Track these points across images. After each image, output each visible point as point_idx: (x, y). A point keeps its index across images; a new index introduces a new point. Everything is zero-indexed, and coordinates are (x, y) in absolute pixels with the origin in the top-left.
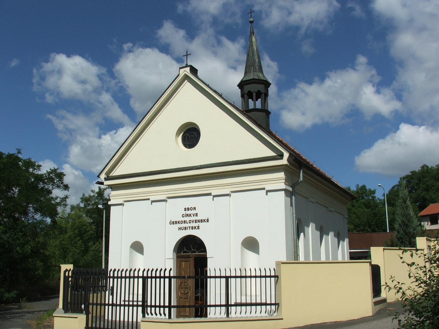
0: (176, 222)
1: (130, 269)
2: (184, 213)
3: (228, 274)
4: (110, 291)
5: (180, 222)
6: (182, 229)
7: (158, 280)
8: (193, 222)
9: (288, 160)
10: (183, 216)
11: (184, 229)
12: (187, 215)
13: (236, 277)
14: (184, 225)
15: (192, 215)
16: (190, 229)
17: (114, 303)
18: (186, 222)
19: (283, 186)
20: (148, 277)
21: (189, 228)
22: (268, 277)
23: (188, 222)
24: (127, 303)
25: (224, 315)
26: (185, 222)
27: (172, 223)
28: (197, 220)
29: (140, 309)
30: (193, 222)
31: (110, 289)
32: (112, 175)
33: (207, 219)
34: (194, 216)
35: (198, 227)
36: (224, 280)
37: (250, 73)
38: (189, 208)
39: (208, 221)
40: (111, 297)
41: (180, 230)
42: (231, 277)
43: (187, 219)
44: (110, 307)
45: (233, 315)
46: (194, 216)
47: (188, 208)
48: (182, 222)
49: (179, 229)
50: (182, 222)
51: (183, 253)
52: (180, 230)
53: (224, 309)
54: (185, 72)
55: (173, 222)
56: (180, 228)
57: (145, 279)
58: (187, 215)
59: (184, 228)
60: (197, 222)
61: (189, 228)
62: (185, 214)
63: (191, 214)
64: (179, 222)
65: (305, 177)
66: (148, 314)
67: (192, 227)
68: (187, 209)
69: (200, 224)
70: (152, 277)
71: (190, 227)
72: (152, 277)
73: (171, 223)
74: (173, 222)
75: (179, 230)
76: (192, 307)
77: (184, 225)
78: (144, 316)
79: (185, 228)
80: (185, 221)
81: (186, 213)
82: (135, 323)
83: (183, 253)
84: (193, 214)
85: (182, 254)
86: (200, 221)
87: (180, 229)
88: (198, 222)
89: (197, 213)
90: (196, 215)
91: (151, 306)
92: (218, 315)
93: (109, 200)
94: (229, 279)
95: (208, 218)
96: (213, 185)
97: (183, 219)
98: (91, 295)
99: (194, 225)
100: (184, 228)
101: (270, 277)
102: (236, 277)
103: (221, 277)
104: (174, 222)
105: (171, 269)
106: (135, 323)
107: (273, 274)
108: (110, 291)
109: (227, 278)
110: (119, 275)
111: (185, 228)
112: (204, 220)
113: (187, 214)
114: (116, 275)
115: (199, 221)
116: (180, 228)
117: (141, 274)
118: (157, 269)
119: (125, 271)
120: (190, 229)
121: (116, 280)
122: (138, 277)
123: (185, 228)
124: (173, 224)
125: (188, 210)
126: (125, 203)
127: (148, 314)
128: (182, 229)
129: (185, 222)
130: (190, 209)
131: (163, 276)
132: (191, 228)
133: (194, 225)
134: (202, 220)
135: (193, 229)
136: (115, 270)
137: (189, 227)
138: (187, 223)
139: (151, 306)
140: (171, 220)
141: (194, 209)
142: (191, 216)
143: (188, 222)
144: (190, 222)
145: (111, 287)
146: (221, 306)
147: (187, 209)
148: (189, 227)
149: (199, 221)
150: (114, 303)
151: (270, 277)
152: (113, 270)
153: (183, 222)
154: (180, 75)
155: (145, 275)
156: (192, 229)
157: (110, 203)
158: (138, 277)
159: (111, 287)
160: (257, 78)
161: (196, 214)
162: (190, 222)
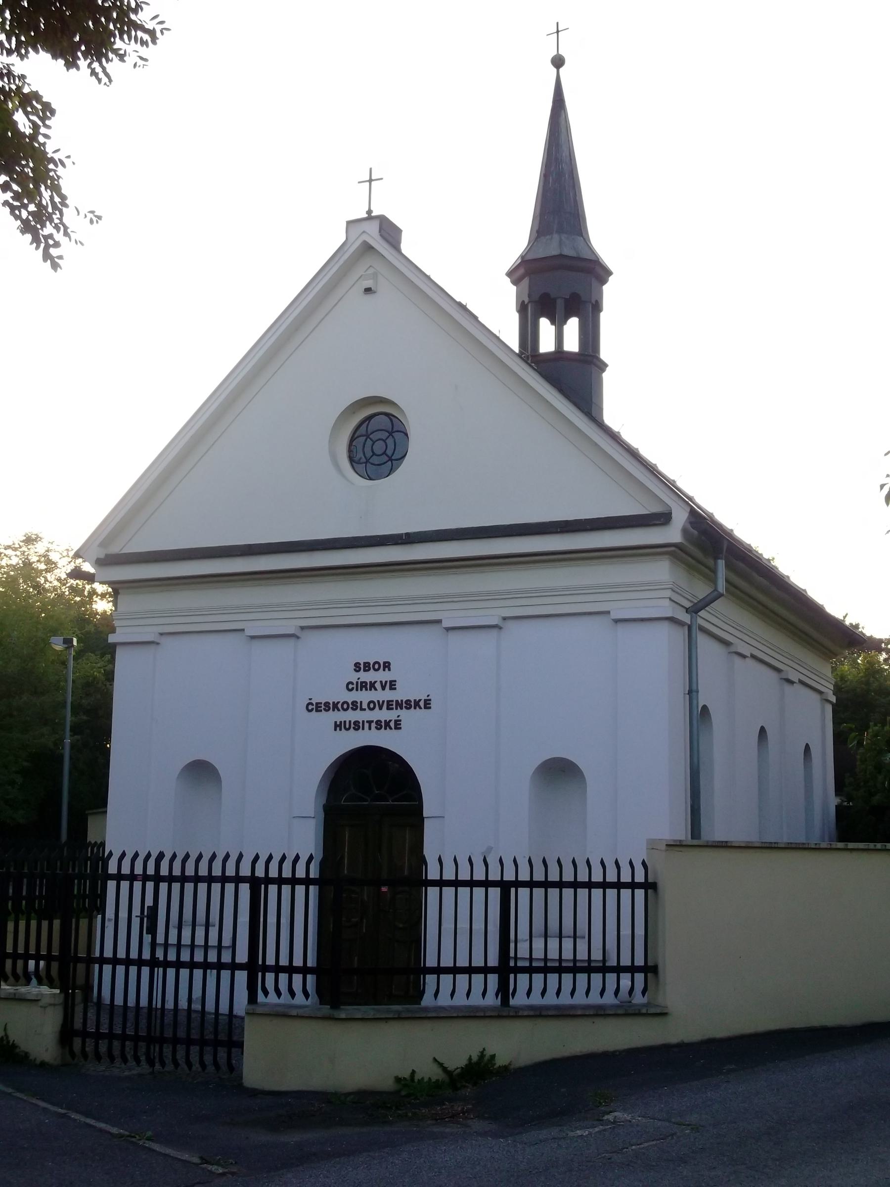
0: (327, 704)
1: (225, 854)
2: (354, 677)
3: (509, 876)
4: (145, 919)
5: (339, 706)
6: (347, 726)
7: (216, 887)
8: (381, 708)
9: (685, 531)
10: (350, 686)
11: (352, 728)
12: (363, 686)
13: (531, 884)
14: (351, 716)
15: (378, 685)
16: (370, 729)
17: (158, 958)
18: (359, 705)
19: (666, 609)
20: (268, 881)
21: (368, 724)
22: (464, 884)
23: (365, 706)
24: (185, 957)
25: (492, 1000)
26: (355, 706)
27: (314, 707)
28: (393, 701)
29: (242, 976)
30: (381, 708)
31: (146, 914)
32: (121, 550)
33: (425, 701)
34: (383, 688)
35: (398, 725)
36: (495, 893)
37: (548, 237)
38: (369, 663)
39: (427, 704)
40: (147, 938)
41: (338, 728)
42: (518, 884)
43: (364, 697)
44: (145, 970)
45: (519, 1000)
46: (383, 688)
47: (365, 663)
48: (345, 706)
49: (338, 726)
50: (345, 706)
51: (344, 802)
52: (338, 728)
53: (493, 980)
54: (365, 237)
55: (317, 704)
56: (338, 723)
57: (255, 883)
58: (363, 686)
59: (352, 726)
60: (394, 706)
61: (366, 725)
62: (357, 682)
63: (375, 682)
64: (335, 706)
65: (736, 587)
66: (266, 993)
67: (378, 722)
68: (362, 666)
69: (404, 714)
70: (280, 881)
71: (373, 721)
72: (280, 881)
73: (313, 709)
74: (318, 705)
75: (335, 730)
76: (164, 1011)
77: (351, 716)
78: (252, 998)
79: (357, 726)
80: (354, 703)
81: (359, 681)
82: (223, 1020)
83: (344, 802)
84: (381, 682)
85: (342, 803)
86: (404, 705)
87: (340, 726)
88: (396, 709)
89: (395, 681)
90: (391, 685)
91: (277, 969)
92: (476, 999)
93: (113, 630)
94: (513, 890)
95: (428, 696)
96: (448, 596)
97: (351, 697)
98: (10, 926)
99: (384, 715)
100: (352, 726)
101: (633, 886)
102: (531, 884)
103: (486, 884)
104: (321, 703)
105: (311, 858)
106: (223, 1020)
107: (640, 878)
108: (145, 919)
109: (505, 887)
110: (177, 872)
111: (357, 726)
112: (417, 704)
113: (362, 683)
114: (164, 871)
115: (399, 705)
116: (338, 723)
117: (245, 871)
118: (257, 854)
119: (156, 860)
120: (370, 729)
121: (163, 886)
122: (238, 880)
123: (356, 723)
124: (317, 711)
125: (365, 670)
126: (164, 640)
127: (266, 993)
128: (347, 726)
129: (355, 706)
130: (371, 666)
131: (129, 873)
132: (373, 725)
133: (384, 715)
134: (408, 702)
135: (380, 729)
136: (161, 856)
137: (370, 722)
138: (362, 709)
139: (277, 969)
140: (310, 699)
141: (386, 667)
142: (376, 689)
143: (365, 706)
144: (372, 706)
145: (148, 907)
146: (485, 970)
147: (362, 666)
148: (367, 722)
149: (399, 705)
150: (158, 958)
151: (633, 886)
152: (154, 855)
153: (351, 706)
154: (351, 240)
155: (260, 873)
156: (376, 728)
157: (112, 639)
158: (238, 880)
159: (148, 907)
160: (571, 253)
161: (391, 682)
162: (372, 706)
